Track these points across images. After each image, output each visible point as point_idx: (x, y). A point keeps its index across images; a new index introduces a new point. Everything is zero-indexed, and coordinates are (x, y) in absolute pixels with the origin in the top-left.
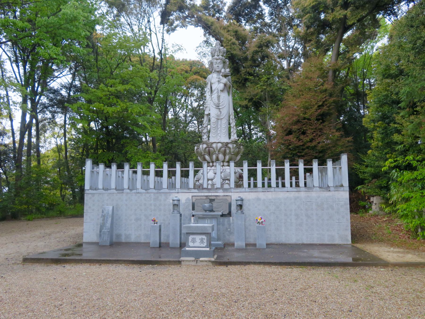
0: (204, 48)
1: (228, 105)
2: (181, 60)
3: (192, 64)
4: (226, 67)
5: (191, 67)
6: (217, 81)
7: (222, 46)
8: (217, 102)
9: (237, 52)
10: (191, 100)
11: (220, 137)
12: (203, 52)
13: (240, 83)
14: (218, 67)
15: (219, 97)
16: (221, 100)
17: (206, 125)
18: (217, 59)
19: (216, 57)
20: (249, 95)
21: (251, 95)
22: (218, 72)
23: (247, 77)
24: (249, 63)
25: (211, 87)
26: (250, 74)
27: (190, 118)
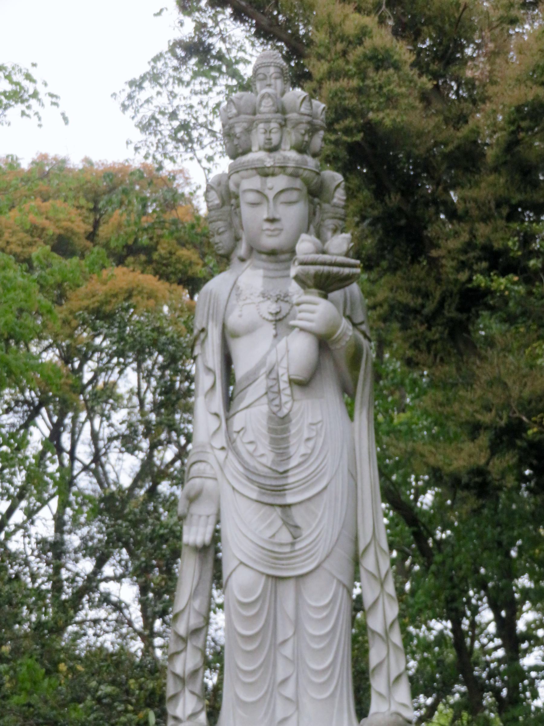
0: (180, 90)
2: (25, 165)
3: (103, 190)
4: (330, 223)
5: (95, 210)
6: (265, 319)
7: (299, 78)
8: (268, 459)
9: (404, 113)
10: (95, 436)
11: (295, 702)
12: (173, 115)
13: (429, 321)
14: (272, 220)
15: (280, 427)
16: (298, 450)
17: (194, 621)
18: (265, 173)
19: (257, 155)
20: (495, 397)
21: (507, 406)
22: (273, 253)
23: (480, 280)
24: (488, 187)
25: (228, 361)
26: (498, 261)
27: (87, 566)
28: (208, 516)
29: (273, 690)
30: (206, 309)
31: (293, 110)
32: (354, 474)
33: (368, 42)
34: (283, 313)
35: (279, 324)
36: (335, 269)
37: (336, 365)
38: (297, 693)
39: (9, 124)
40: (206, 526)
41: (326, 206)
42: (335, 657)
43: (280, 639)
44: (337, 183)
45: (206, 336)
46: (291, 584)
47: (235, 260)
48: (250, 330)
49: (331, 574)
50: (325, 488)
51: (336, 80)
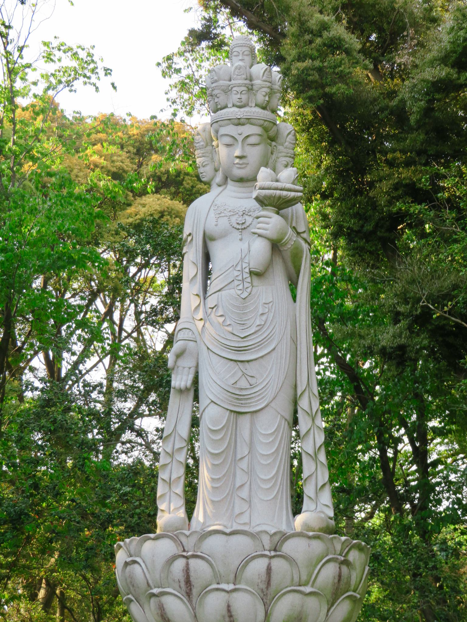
1: (285, 349)
11: (249, 502)
22: (241, 180)
25: (207, 258)
28: (190, 368)
29: (233, 493)
30: (192, 220)
31: (258, 78)
32: (295, 340)
33: (325, 34)
34: (247, 224)
35: (244, 231)
36: (285, 193)
37: (284, 261)
38: (250, 496)
39: (75, 91)
40: (188, 375)
41: (281, 148)
42: (278, 471)
43: (239, 456)
44: (288, 131)
45: (192, 239)
46: (248, 416)
47: (214, 185)
48: (224, 235)
49: (277, 411)
50: (274, 349)
51: (304, 61)
